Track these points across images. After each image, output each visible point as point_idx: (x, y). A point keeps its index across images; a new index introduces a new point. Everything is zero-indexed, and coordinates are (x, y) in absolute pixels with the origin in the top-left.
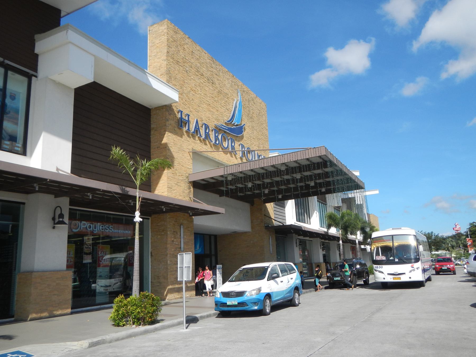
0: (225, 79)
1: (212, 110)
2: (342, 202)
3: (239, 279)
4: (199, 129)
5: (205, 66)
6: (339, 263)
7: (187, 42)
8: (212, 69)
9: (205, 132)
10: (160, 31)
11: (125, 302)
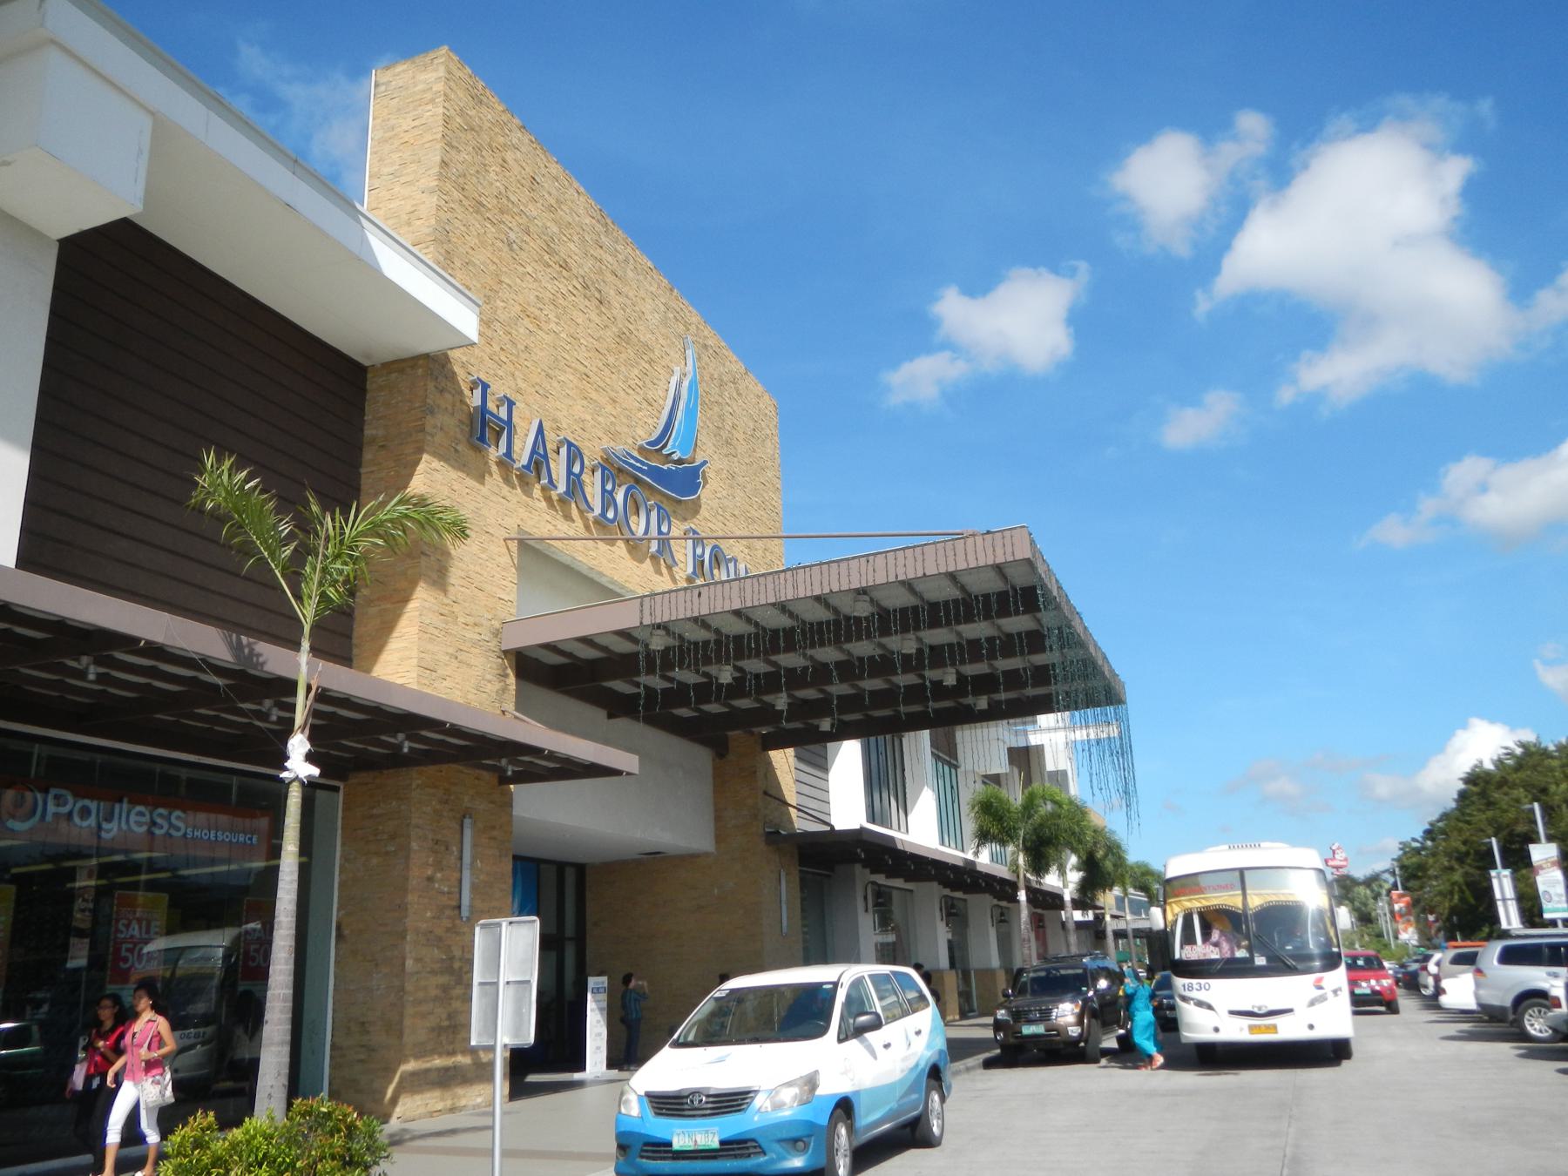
0: (642, 293)
1: (594, 395)
2: (1011, 761)
3: (711, 1035)
4: (545, 456)
5: (575, 238)
6: (1060, 972)
7: (515, 141)
8: (598, 253)
10: (420, 87)
11: (219, 1146)
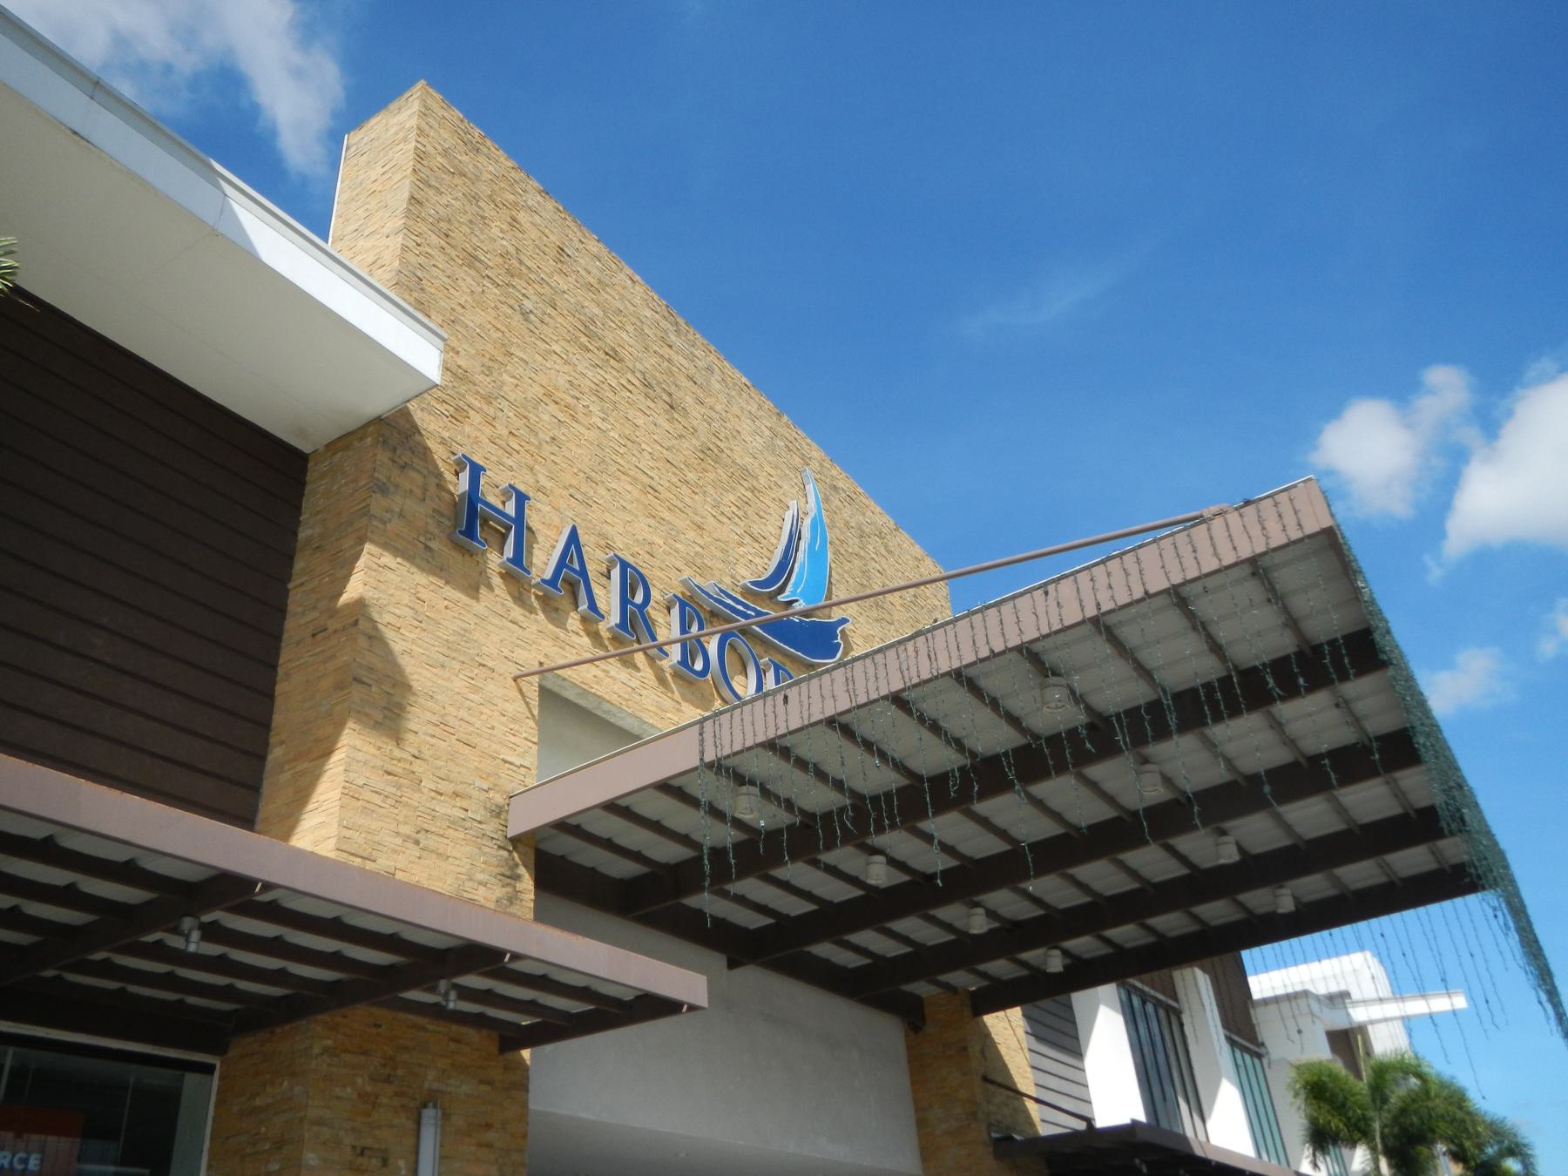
1: (666, 515)
9: (624, 602)
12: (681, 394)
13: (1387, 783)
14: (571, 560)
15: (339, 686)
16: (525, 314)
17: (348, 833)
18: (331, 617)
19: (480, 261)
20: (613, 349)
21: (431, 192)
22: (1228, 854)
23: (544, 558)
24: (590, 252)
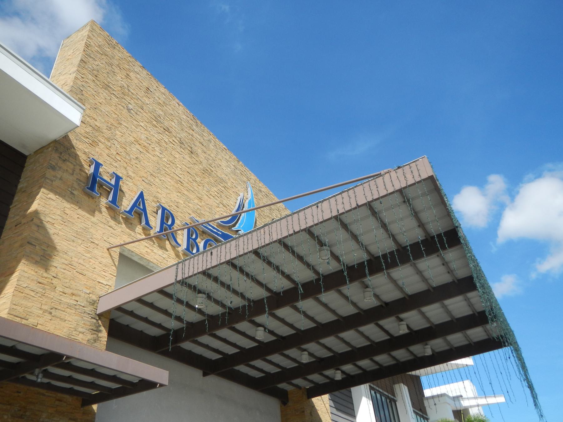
1: (186, 192)
4: (144, 209)
9: (162, 223)
12: (196, 148)
13: (438, 256)
14: (139, 205)
15: (21, 246)
16: (129, 110)
17: (15, 307)
18: (24, 218)
19: (111, 88)
20: (167, 128)
21: (91, 59)
22: (403, 330)
23: (128, 203)
24: (160, 92)
